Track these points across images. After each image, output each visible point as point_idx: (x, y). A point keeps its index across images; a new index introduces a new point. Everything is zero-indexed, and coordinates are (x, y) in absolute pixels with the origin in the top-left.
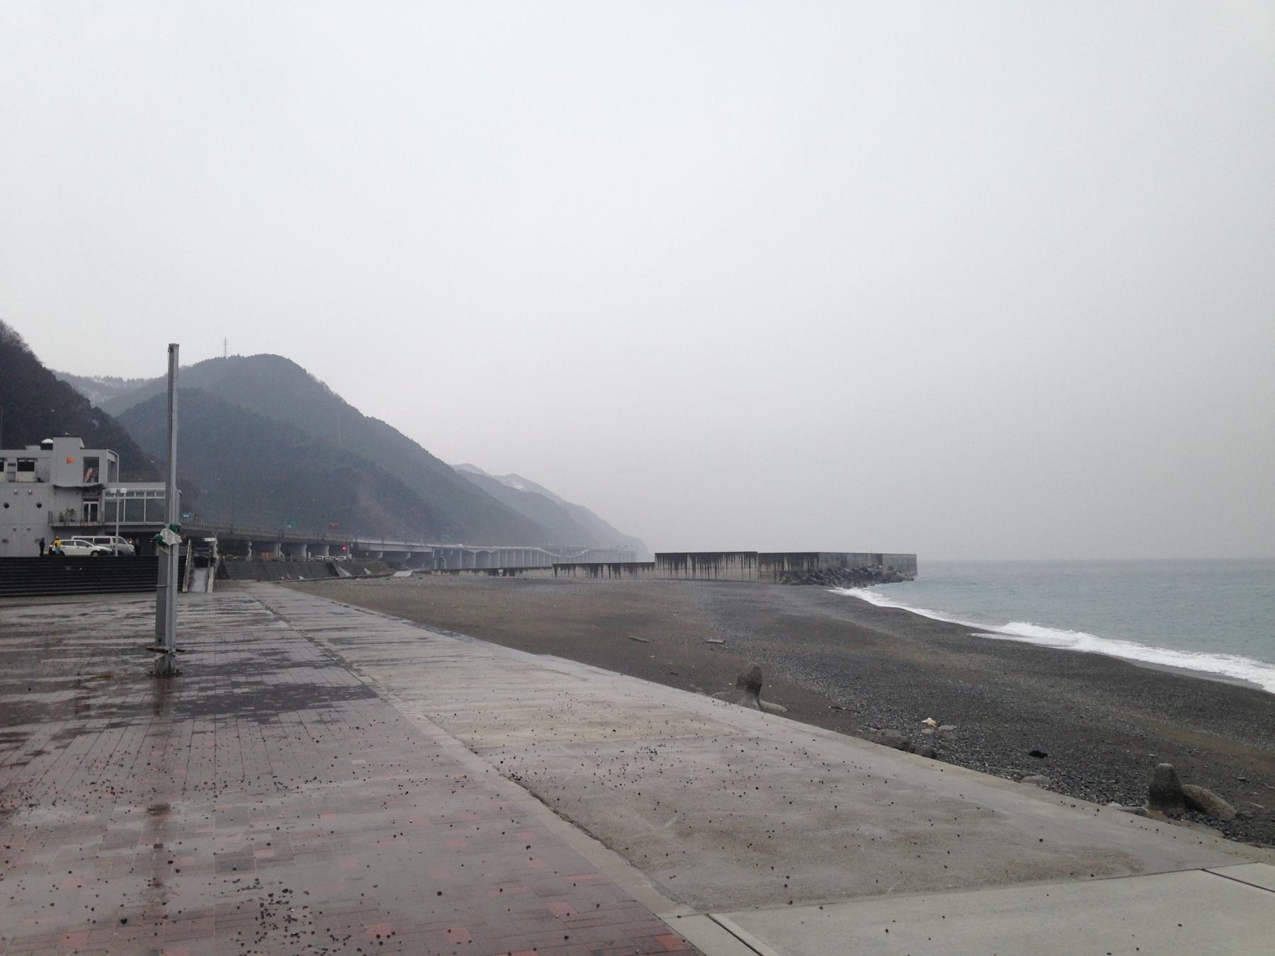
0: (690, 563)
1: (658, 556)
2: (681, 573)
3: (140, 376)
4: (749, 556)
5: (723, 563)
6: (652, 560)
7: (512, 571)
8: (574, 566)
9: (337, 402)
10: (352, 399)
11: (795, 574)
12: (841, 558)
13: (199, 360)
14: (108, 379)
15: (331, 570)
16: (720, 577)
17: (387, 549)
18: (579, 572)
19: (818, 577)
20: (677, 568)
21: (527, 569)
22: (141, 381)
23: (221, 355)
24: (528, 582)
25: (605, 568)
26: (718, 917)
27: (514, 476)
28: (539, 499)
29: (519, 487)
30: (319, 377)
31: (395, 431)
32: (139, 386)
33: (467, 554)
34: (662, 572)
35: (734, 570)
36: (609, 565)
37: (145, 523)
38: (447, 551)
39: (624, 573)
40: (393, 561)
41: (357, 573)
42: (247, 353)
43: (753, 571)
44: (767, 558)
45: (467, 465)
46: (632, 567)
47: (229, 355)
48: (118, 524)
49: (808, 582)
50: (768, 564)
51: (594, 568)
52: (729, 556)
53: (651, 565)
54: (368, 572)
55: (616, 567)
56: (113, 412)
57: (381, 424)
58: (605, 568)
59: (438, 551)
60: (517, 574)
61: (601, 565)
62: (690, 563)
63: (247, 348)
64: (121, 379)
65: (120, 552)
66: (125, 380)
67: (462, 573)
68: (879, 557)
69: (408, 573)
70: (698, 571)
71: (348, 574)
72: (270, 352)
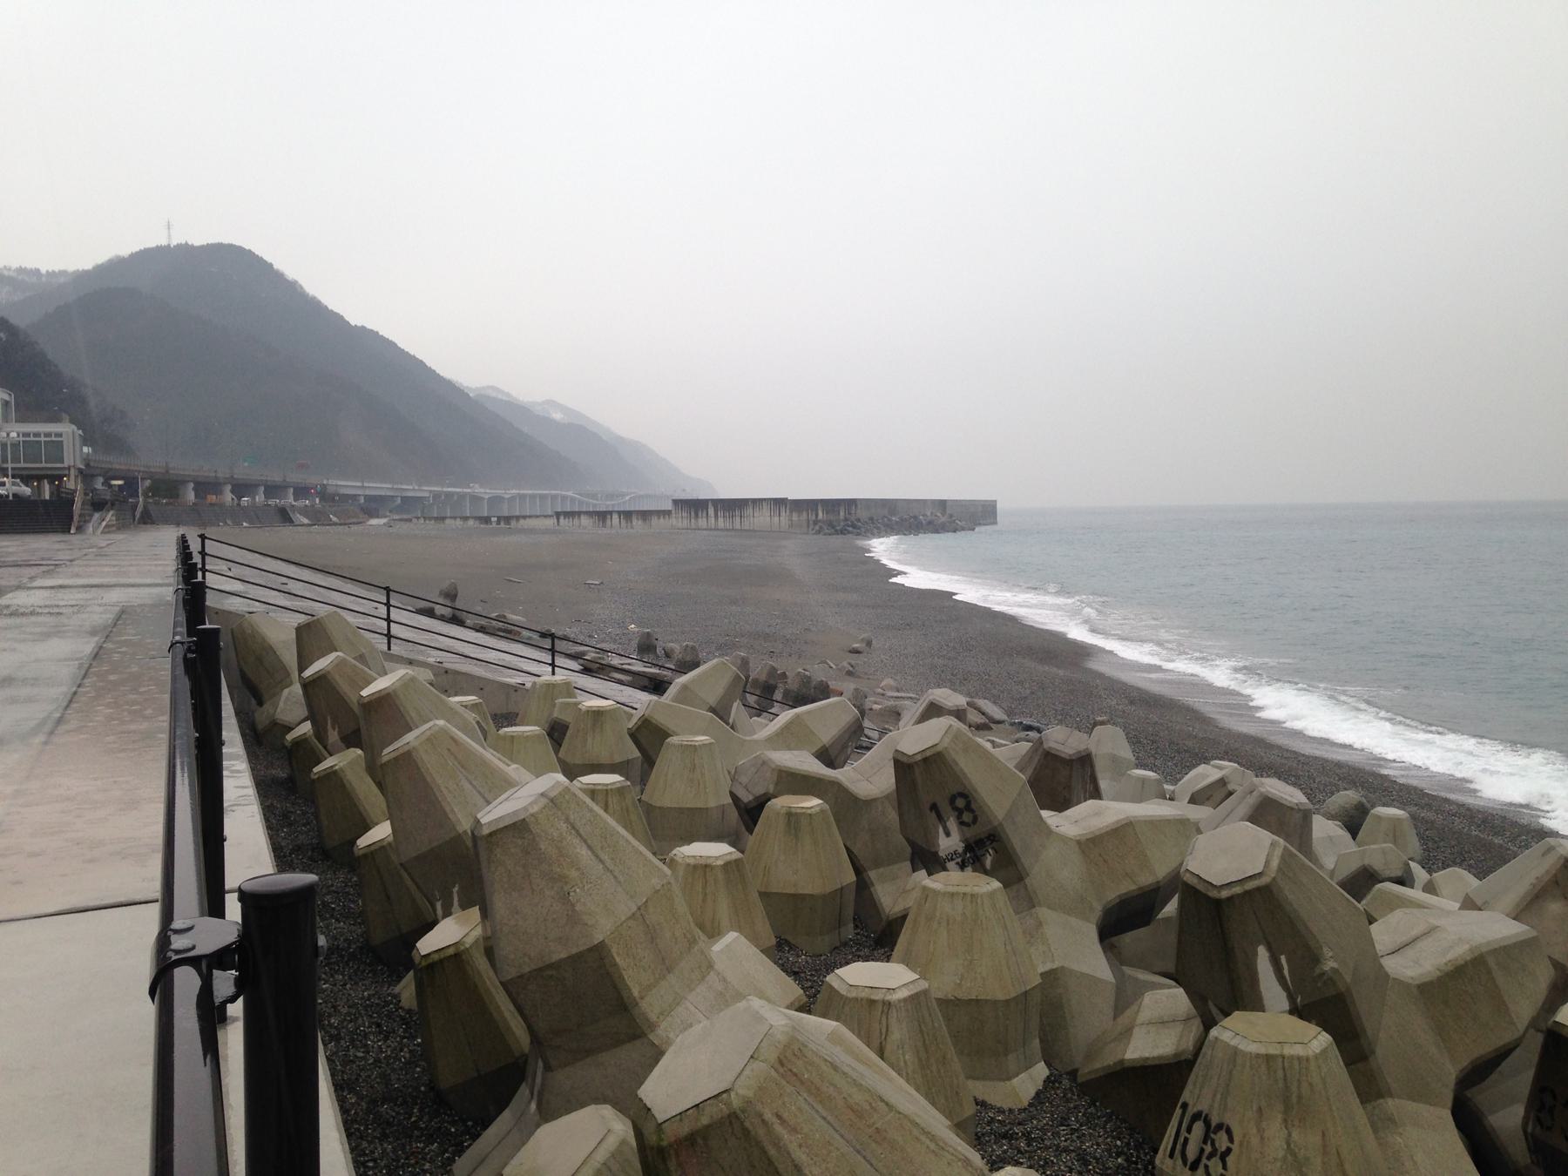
0: (711, 511)
1: (676, 502)
2: (702, 522)
3: (62, 268)
4: (779, 503)
5: (749, 511)
6: (669, 506)
7: (508, 519)
8: (579, 513)
9: (315, 308)
10: (333, 302)
11: (831, 525)
12: (889, 505)
13: (136, 249)
14: (21, 270)
15: (285, 516)
16: (746, 526)
17: (368, 492)
18: (585, 520)
19: (854, 526)
20: (697, 516)
21: (524, 517)
22: (63, 273)
23: (164, 242)
24: (532, 531)
25: (615, 516)
26: (36, 584)
27: (551, 403)
28: (581, 432)
29: (557, 416)
30: (291, 273)
31: (392, 345)
32: (62, 280)
33: (476, 499)
34: (679, 521)
35: (761, 519)
36: (619, 513)
37: (44, 465)
38: (449, 495)
39: (637, 522)
40: (373, 506)
41: (318, 518)
42: (198, 240)
43: (784, 519)
44: (799, 505)
45: (492, 387)
46: (645, 515)
47: (174, 243)
48: (10, 465)
49: (842, 532)
50: (800, 512)
51: (602, 516)
52: (757, 502)
53: (667, 513)
54: (335, 519)
55: (627, 515)
56: (19, 320)
57: (374, 335)
58: (615, 516)
59: (436, 496)
60: (513, 523)
61: (611, 513)
62: (711, 511)
63: (199, 237)
64: (38, 271)
65: (15, 495)
66: (43, 271)
67: (448, 521)
68: (942, 504)
69: (382, 521)
70: (721, 520)
71: (306, 521)
72: (226, 241)
